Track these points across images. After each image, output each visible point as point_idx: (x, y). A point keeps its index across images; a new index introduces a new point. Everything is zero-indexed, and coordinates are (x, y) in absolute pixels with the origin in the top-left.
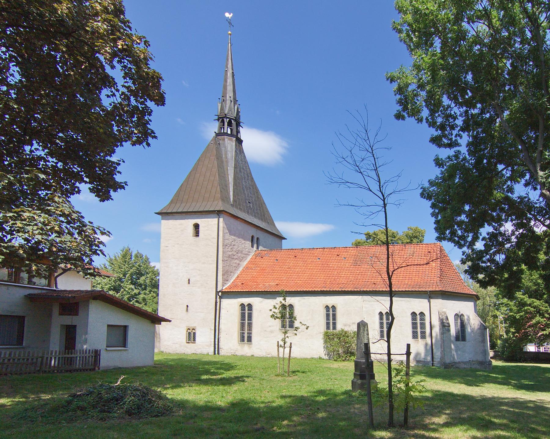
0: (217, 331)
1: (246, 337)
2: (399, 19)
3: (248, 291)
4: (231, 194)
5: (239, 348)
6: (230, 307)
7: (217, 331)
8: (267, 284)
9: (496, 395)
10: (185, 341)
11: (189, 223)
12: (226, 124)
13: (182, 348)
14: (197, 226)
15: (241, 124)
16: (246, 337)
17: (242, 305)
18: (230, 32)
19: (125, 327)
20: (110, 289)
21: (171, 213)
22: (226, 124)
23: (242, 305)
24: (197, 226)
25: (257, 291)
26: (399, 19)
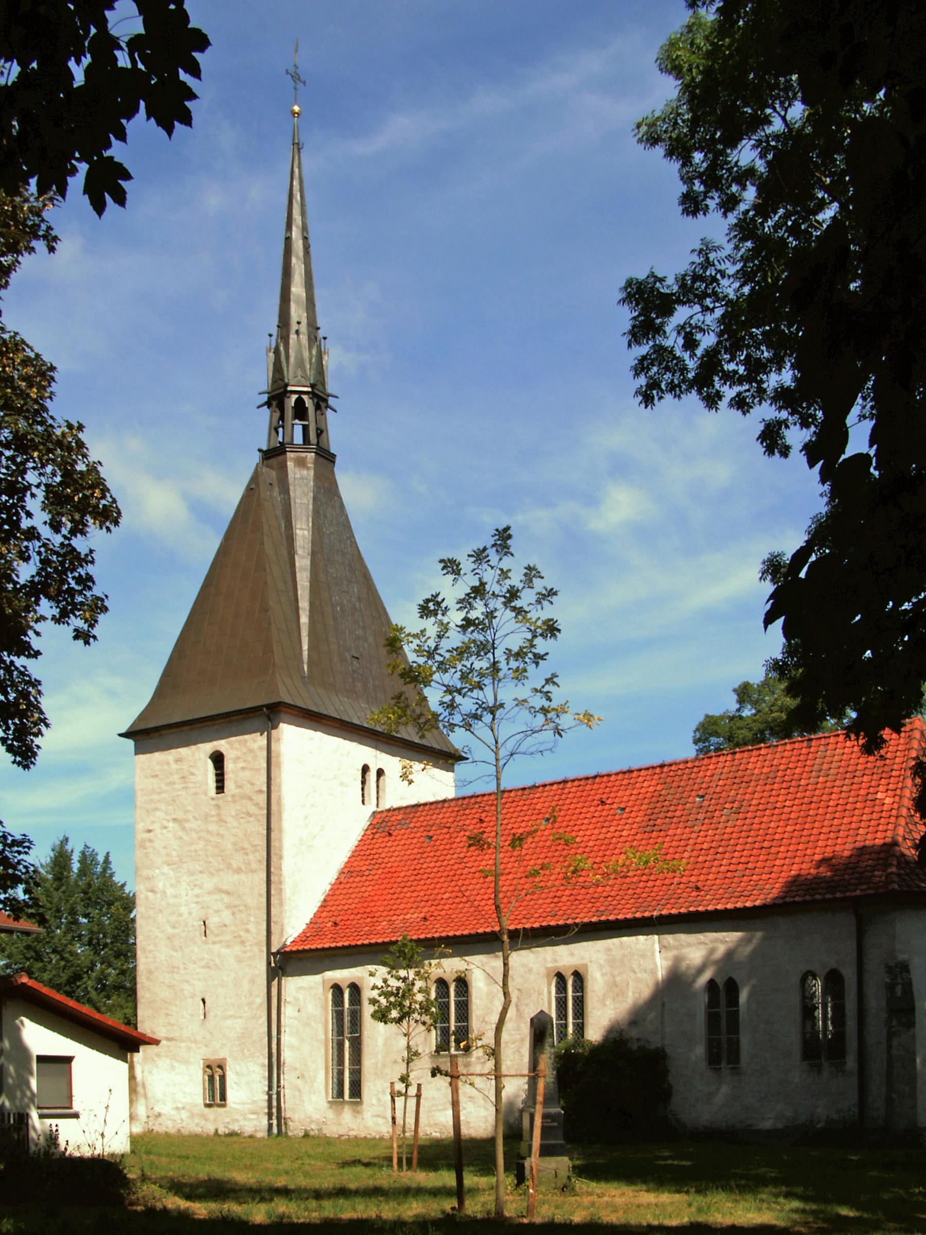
0: (274, 1065)
1: (349, 1087)
2: (112, 527)
3: (350, 947)
4: (305, 647)
5: (330, 1114)
6: (307, 994)
7: (274, 1065)
8: (398, 923)
9: (845, 848)
10: (200, 1101)
11: (197, 755)
12: (289, 413)
13: (196, 1121)
14: (218, 759)
15: (331, 401)
16: (349, 1087)
17: (337, 989)
18: (296, 108)
19: (68, 1060)
20: (308, 469)
21: (157, 729)
22: (289, 413)
23: (337, 989)
24: (218, 759)
25: (370, 945)
26: (112, 527)
